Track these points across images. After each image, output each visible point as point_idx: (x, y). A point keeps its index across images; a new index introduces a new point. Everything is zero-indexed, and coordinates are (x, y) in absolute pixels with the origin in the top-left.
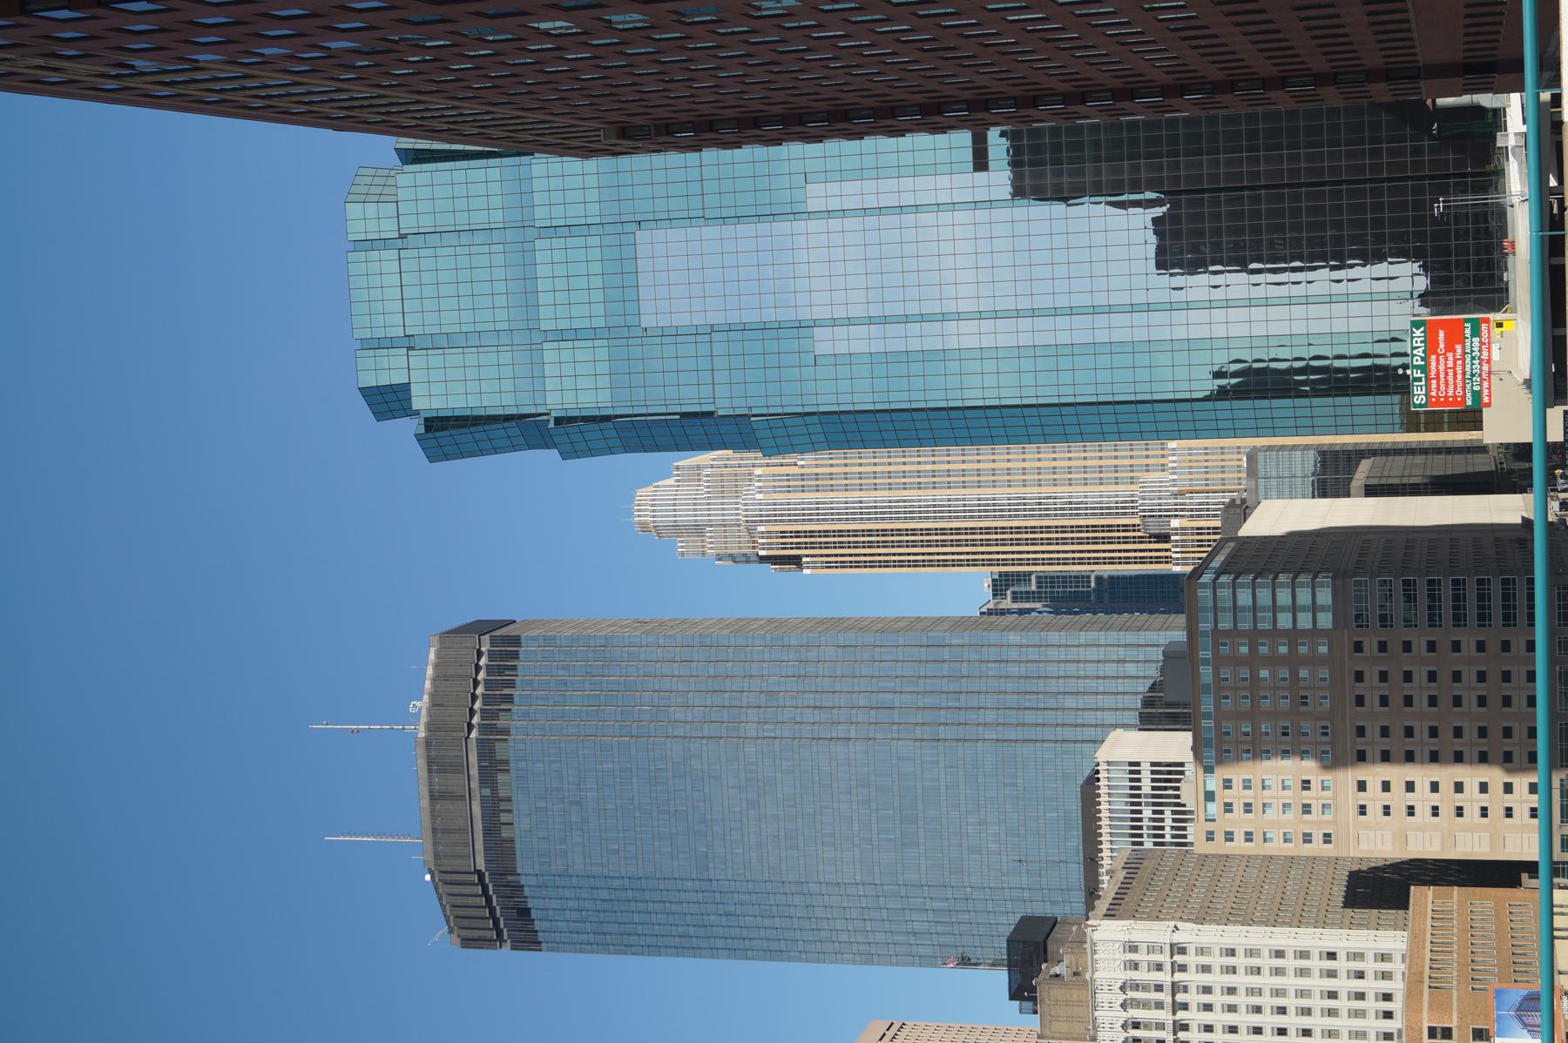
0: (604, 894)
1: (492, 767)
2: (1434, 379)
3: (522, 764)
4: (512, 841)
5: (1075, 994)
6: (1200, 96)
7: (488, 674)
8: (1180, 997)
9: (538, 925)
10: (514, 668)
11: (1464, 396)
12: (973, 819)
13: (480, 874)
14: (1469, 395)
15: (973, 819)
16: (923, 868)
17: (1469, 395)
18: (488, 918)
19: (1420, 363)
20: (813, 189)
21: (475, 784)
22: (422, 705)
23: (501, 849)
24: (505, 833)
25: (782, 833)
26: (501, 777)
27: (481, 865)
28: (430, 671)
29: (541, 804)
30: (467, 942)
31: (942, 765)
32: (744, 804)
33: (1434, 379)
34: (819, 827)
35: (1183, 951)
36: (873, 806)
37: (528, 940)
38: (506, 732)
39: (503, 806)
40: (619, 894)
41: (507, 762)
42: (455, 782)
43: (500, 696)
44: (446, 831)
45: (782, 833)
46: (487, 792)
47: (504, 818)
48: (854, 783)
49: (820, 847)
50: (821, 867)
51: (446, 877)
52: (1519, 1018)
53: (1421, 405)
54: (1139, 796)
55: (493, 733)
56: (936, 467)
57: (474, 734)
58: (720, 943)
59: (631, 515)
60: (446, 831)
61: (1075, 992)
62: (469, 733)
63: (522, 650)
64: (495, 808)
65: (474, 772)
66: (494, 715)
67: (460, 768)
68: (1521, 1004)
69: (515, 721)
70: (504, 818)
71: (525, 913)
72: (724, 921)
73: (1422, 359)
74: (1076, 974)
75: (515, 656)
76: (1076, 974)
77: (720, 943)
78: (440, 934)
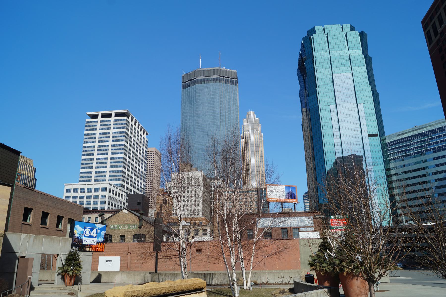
0: (192, 99)
1: (215, 80)
3: (215, 85)
4: (202, 83)
7: (230, 80)
8: (190, 187)
9: (186, 88)
10: (231, 84)
11: (333, 226)
13: (196, 78)
14: (333, 227)
16: (198, 153)
17: (333, 227)
19: (339, 217)
20: (362, 105)
21: (211, 77)
22: (224, 68)
23: (200, 82)
24: (203, 82)
25: (204, 129)
26: (213, 81)
27: (197, 78)
28: (230, 70)
29: (208, 88)
30: (183, 77)
32: (209, 122)
35: (198, 188)
37: (184, 87)
38: (221, 83)
39: (208, 82)
40: (192, 102)
41: (215, 82)
42: (212, 73)
43: (226, 82)
44: (203, 73)
45: (204, 129)
46: (210, 79)
47: (208, 82)
51: (196, 73)
52: (290, 192)
53: (331, 218)
54: (216, 187)
55: (220, 80)
56: (260, 162)
57: (220, 77)
58: (184, 119)
59: (250, 111)
60: (203, 73)
62: (221, 76)
63: (234, 85)
64: (208, 81)
65: (214, 77)
66: (223, 81)
67: (214, 75)
68: (293, 193)
69: (222, 84)
70: (206, 82)
71: (189, 86)
72: (188, 120)
73: (340, 218)
75: (233, 84)
77: (184, 119)
78: (184, 73)
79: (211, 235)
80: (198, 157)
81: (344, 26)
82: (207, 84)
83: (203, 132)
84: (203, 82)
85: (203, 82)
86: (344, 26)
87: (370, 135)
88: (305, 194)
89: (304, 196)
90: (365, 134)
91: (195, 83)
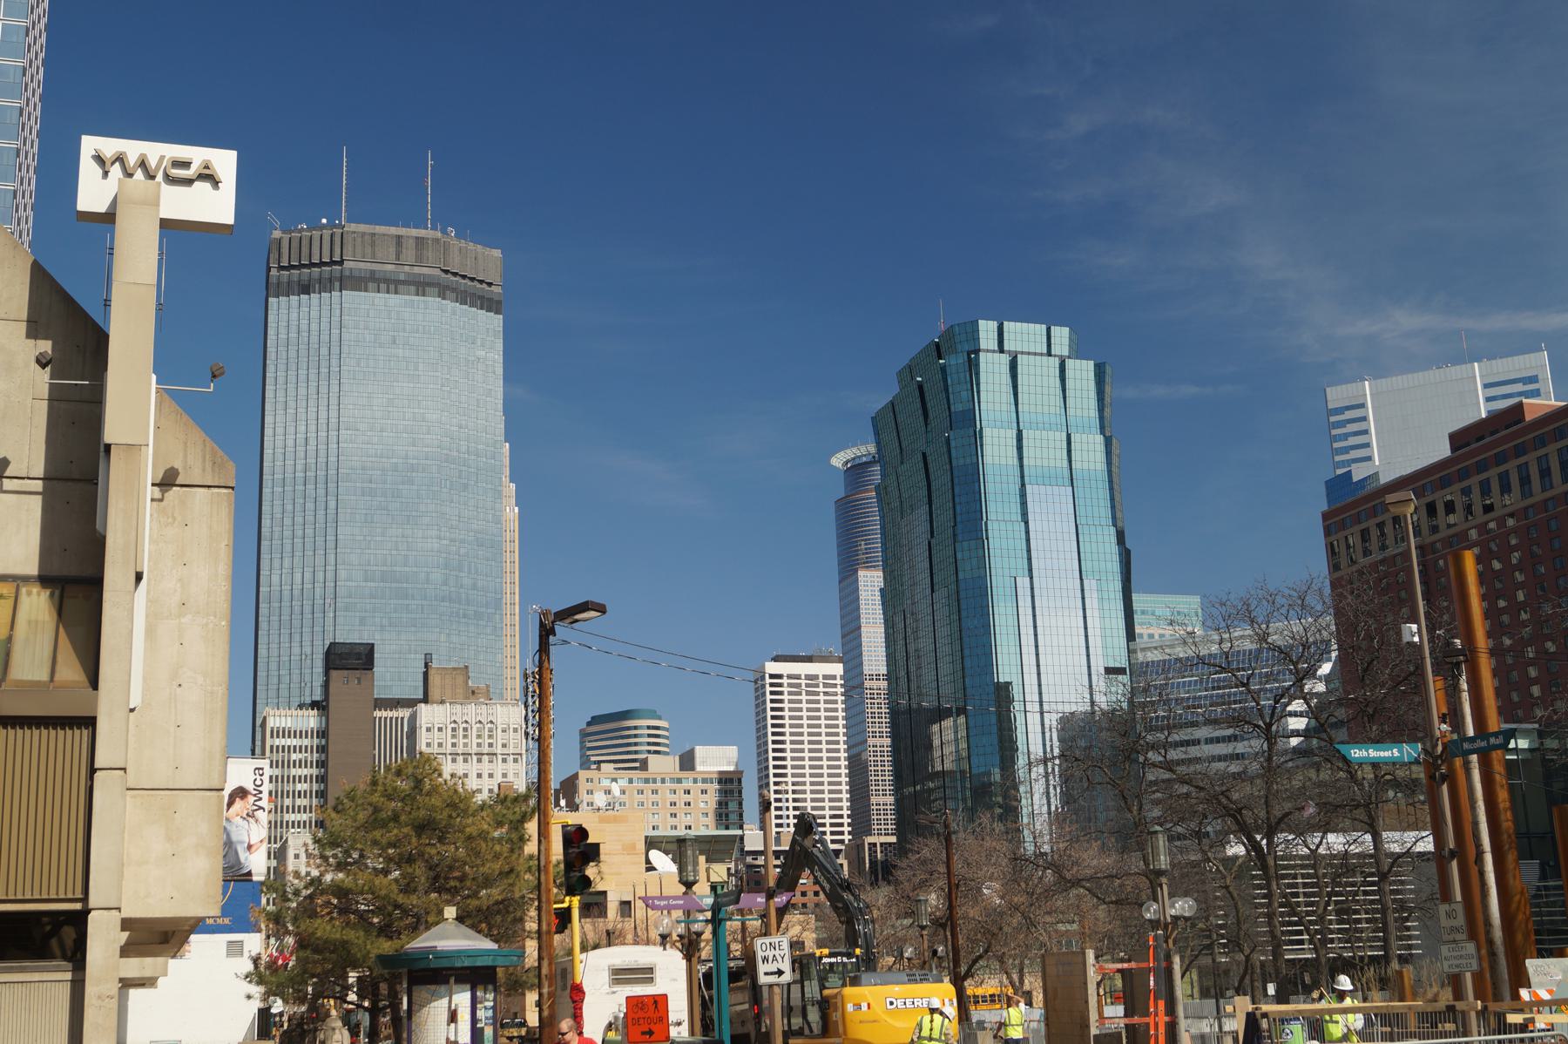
2: (1488, 743)
3: (422, 306)
4: (366, 291)
5: (460, 691)
6: (1465, 696)
8: (486, 758)
9: (294, 298)
12: (385, 622)
15: (385, 622)
16: (348, 583)
18: (300, 262)
20: (1094, 583)
23: (359, 282)
26: (413, 288)
31: (424, 603)
33: (1488, 743)
34: (378, 512)
36: (394, 552)
43: (464, 298)
45: (373, 486)
46: (402, 277)
47: (392, 287)
48: (410, 540)
49: (364, 512)
50: (349, 511)
55: (443, 291)
60: (373, 244)
61: (461, 691)
64: (391, 284)
65: (416, 270)
69: (449, 305)
74: (473, 692)
76: (473, 692)
79: (274, 905)
80: (346, 600)
81: (1055, 330)
82: (387, 295)
83: (368, 498)
84: (370, 285)
85: (370, 285)
86: (1055, 330)
87: (1109, 671)
88: (589, 724)
89: (584, 735)
90: (1098, 666)
91: (337, 284)
